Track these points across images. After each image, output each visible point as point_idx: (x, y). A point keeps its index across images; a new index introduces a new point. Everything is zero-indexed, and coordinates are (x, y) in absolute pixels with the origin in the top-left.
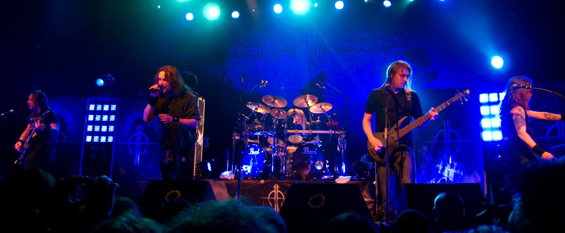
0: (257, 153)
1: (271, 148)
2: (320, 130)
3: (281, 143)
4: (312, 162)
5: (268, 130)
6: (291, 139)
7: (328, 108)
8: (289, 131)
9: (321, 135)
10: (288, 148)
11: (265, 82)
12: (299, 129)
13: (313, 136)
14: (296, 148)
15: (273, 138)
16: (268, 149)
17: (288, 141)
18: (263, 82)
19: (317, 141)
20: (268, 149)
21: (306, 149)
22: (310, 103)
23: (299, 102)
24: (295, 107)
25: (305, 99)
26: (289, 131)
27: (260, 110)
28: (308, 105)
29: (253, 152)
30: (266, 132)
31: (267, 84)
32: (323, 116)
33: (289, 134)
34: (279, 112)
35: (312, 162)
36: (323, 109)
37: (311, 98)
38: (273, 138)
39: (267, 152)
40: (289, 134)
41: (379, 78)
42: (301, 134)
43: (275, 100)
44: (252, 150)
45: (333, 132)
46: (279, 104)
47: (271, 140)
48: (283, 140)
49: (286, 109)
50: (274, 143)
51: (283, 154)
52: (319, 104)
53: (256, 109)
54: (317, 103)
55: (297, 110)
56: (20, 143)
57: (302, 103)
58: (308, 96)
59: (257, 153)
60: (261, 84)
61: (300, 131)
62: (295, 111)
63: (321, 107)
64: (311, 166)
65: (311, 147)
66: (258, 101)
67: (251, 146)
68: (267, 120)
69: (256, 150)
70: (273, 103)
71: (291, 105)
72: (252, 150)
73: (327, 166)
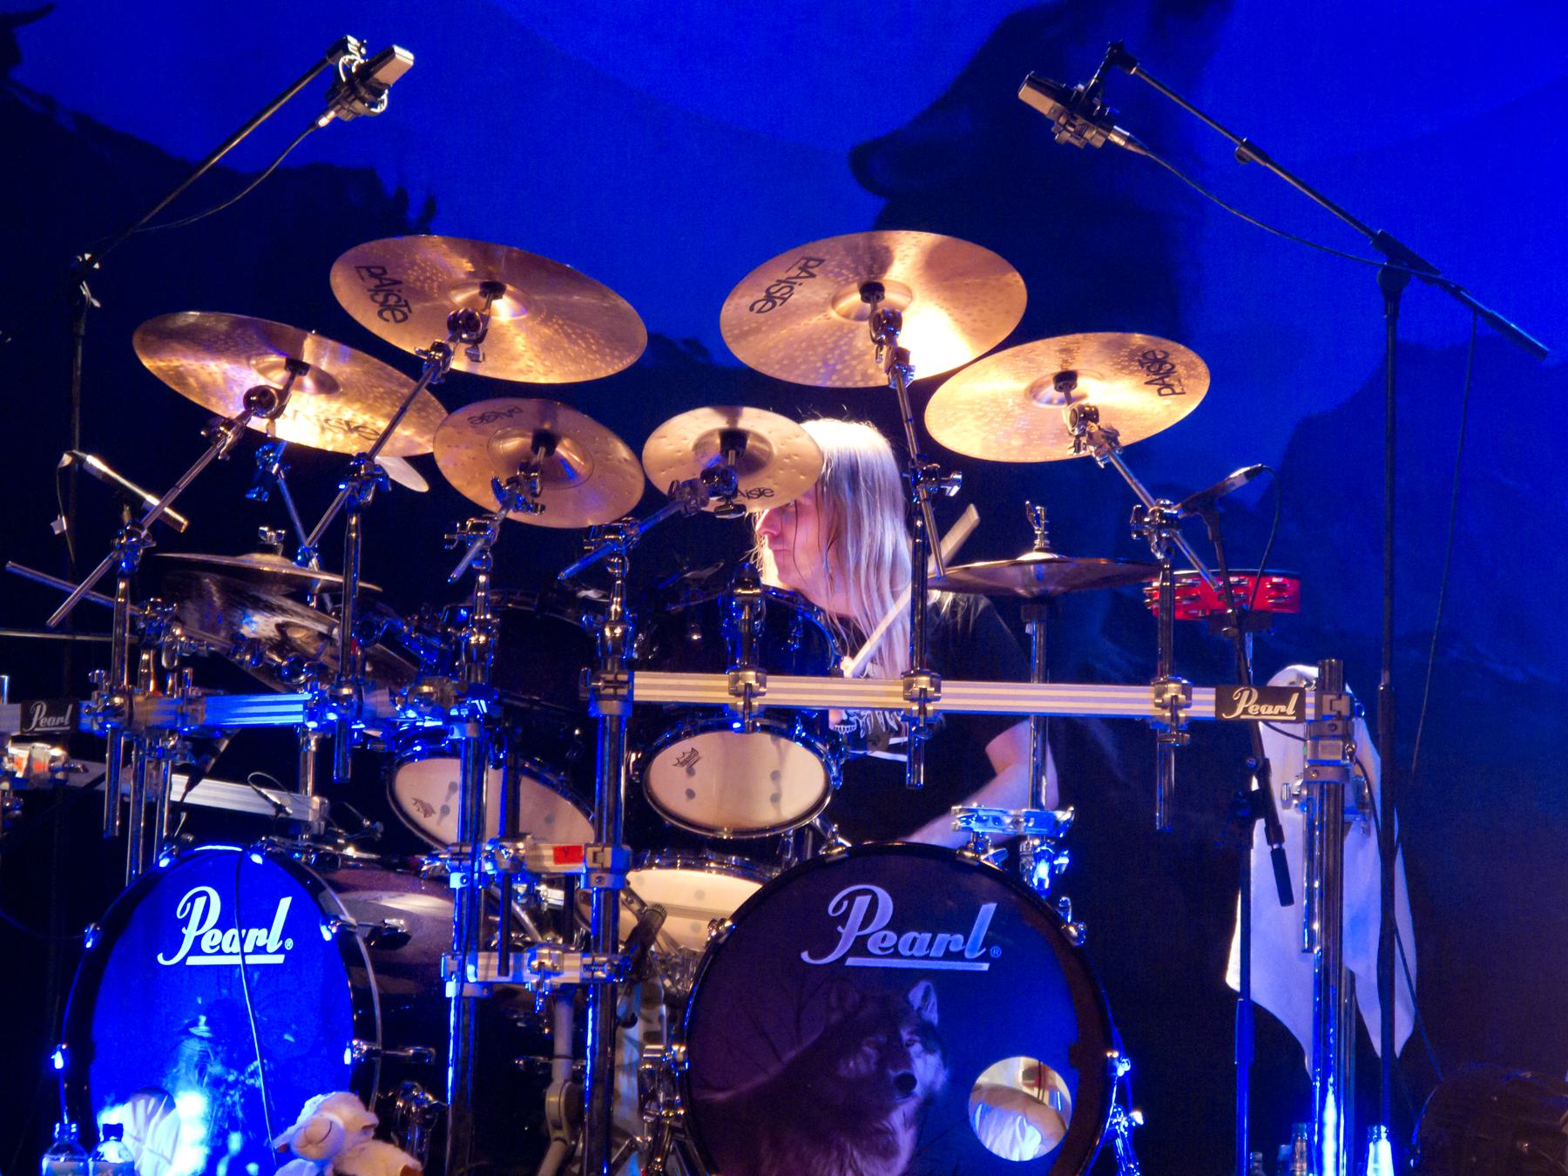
0: (267, 943)
1: (438, 883)
2: (1057, 673)
3: (560, 830)
4: (927, 1068)
5: (393, 676)
6: (686, 781)
7: (1138, 400)
8: (653, 687)
9: (1062, 734)
10: (657, 883)
11: (379, 55)
12: (777, 663)
13: (959, 753)
14: (746, 889)
15: (449, 772)
16: (412, 906)
17: (642, 803)
18: (354, 53)
19: (1011, 807)
20: (412, 906)
21: (866, 920)
22: (934, 335)
23: (791, 316)
24: (743, 387)
25: (872, 290)
26: (653, 687)
27: (309, 422)
28: (900, 359)
29: (209, 937)
30: (379, 700)
31: (405, 87)
32: (1071, 495)
33: (661, 725)
34: (545, 440)
35: (927, 1068)
36: (1086, 416)
37: (936, 270)
38: (449, 772)
39: (388, 939)
40: (661, 725)
41: (753, 567)
42: (806, 725)
43: (493, 289)
44: (202, 909)
45: (1203, 703)
46: (523, 345)
47: (431, 792)
48: (582, 794)
49: (629, 406)
50: (472, 824)
51: (572, 969)
52: (1046, 355)
53: (264, 401)
54: (1026, 332)
55: (759, 422)
56: (388, 74)
57: (841, 336)
58: (908, 251)
59: (267, 943)
60: (329, 90)
61: (786, 690)
62: (733, 439)
63: (1066, 380)
64: (923, 1119)
65: (935, 892)
66: (285, 305)
67: (190, 872)
68: (394, 539)
69: (244, 912)
70: (470, 326)
71: (686, 366)
72: (202, 909)
73: (1126, 1120)
